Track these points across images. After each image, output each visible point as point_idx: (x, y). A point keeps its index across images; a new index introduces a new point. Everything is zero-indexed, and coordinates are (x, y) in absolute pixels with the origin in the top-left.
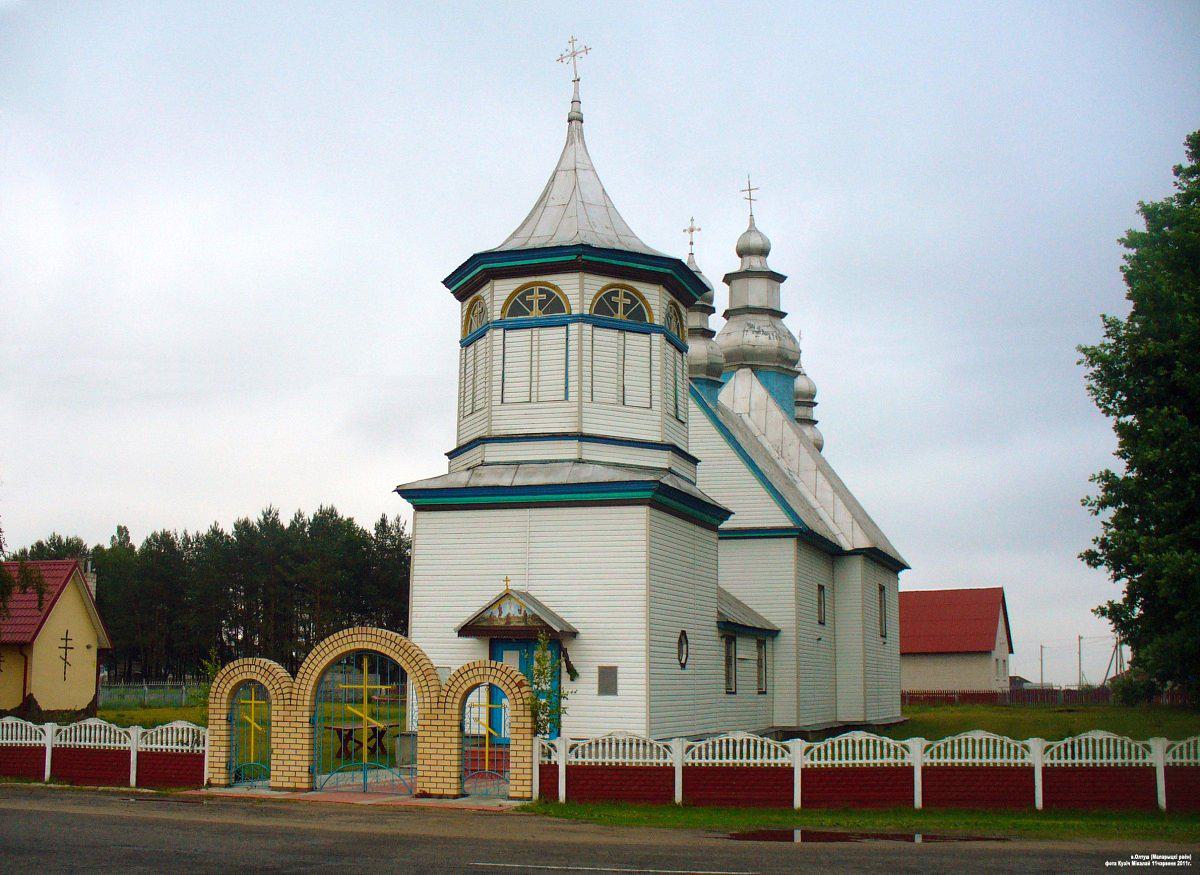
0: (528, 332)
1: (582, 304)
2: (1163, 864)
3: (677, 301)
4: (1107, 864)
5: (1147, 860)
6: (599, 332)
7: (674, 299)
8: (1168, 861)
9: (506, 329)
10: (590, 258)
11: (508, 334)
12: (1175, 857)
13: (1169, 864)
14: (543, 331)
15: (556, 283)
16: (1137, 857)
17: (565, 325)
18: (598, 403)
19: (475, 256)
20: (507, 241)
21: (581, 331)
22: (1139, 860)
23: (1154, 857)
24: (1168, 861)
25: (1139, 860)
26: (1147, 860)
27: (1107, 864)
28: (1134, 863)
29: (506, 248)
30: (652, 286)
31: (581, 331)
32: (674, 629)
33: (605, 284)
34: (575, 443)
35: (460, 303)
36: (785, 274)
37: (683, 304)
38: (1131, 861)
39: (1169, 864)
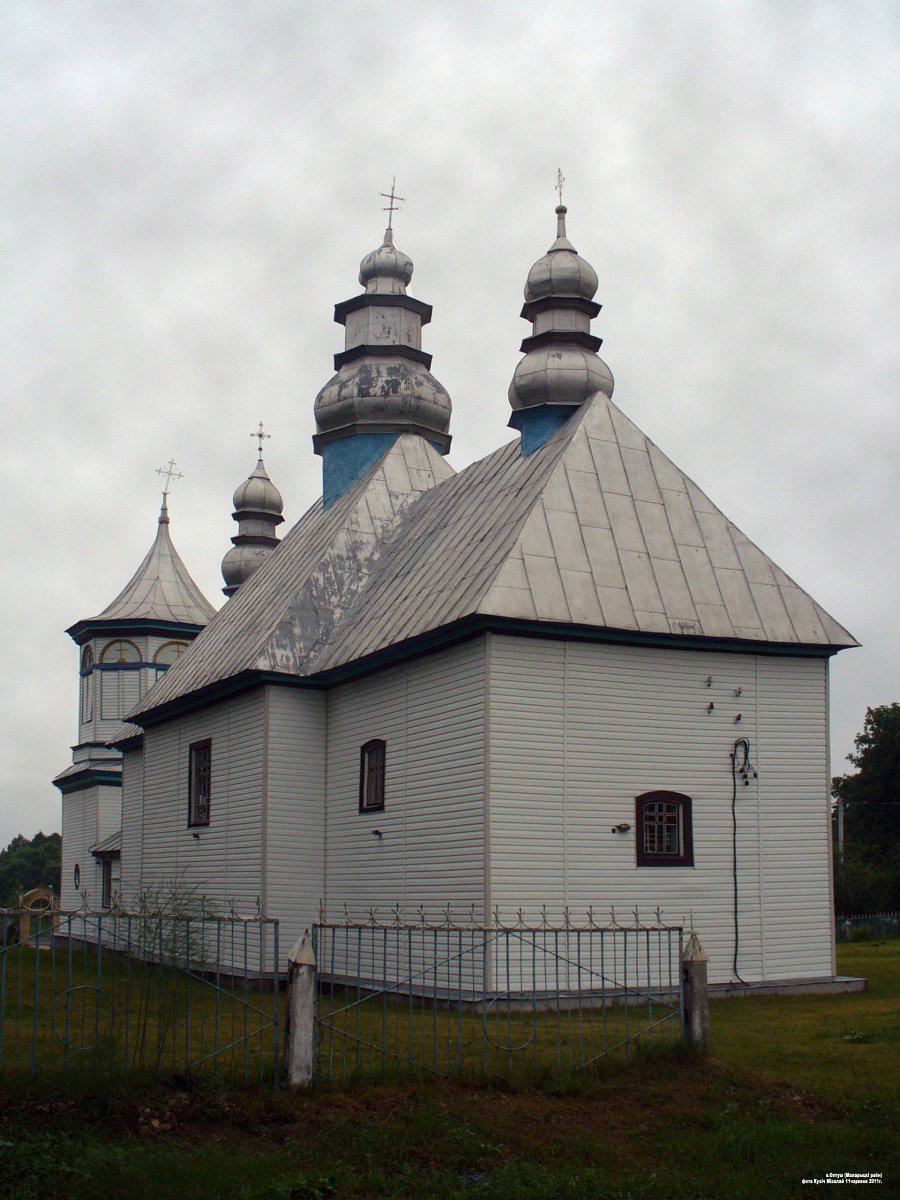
4: (804, 1182)
5: (840, 1178)
12: (867, 1176)
16: (831, 1175)
22: (833, 1178)
23: (847, 1175)
25: (833, 1178)
26: (840, 1178)
27: (804, 1182)
28: (829, 1181)
35: (79, 646)
38: (826, 1179)
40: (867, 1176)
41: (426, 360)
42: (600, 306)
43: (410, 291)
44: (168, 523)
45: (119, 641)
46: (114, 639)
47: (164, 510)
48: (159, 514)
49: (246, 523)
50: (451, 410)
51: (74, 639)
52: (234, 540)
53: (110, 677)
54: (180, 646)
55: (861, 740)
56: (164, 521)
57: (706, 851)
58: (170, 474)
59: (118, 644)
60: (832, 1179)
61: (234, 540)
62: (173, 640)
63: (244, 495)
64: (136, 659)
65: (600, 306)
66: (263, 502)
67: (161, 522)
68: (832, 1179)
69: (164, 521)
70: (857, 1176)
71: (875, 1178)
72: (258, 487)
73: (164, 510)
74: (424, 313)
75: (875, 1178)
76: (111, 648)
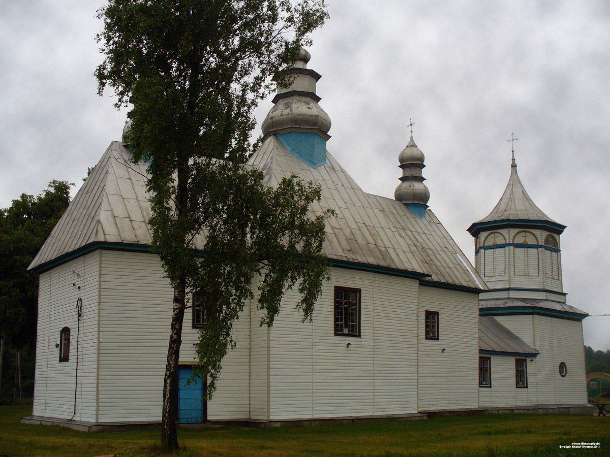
0: (492, 250)
1: (509, 239)
2: (587, 447)
3: (551, 233)
4: (560, 447)
5: (579, 445)
6: (516, 249)
7: (549, 233)
8: (589, 445)
9: (485, 249)
10: (479, 227)
11: (486, 251)
12: (592, 444)
13: (590, 447)
14: (497, 250)
15: (501, 232)
16: (574, 444)
17: (504, 247)
18: (518, 275)
19: (473, 224)
20: (485, 218)
21: (509, 249)
22: (575, 445)
23: (583, 443)
24: (589, 445)
25: (575, 445)
26: (579, 445)
27: (560, 447)
28: (573, 447)
29: (485, 221)
30: (538, 230)
31: (509, 249)
32: (43, 303)
33: (518, 231)
34: (544, 293)
35: (474, 238)
36: (565, 225)
37: (554, 233)
38: (571, 445)
39: (590, 447)
40: (592, 444)
41: (318, 99)
42: (321, 76)
43: (309, 66)
44: (516, 167)
45: (525, 232)
46: (491, 232)
47: (513, 160)
48: (511, 163)
49: (407, 170)
50: (331, 124)
51: (471, 234)
52: (400, 179)
53: (489, 252)
54: (527, 233)
55: (163, 266)
56: (514, 166)
57: (366, 313)
58: (513, 140)
59: (524, 233)
60: (575, 445)
61: (400, 179)
62: (523, 230)
63: (403, 157)
64: (503, 242)
65: (321, 76)
66: (413, 158)
67: (512, 166)
68: (575, 445)
69: (514, 166)
70: (588, 444)
71: (597, 445)
72: (409, 152)
73: (513, 160)
74: (316, 76)
75: (597, 445)
76: (489, 237)
